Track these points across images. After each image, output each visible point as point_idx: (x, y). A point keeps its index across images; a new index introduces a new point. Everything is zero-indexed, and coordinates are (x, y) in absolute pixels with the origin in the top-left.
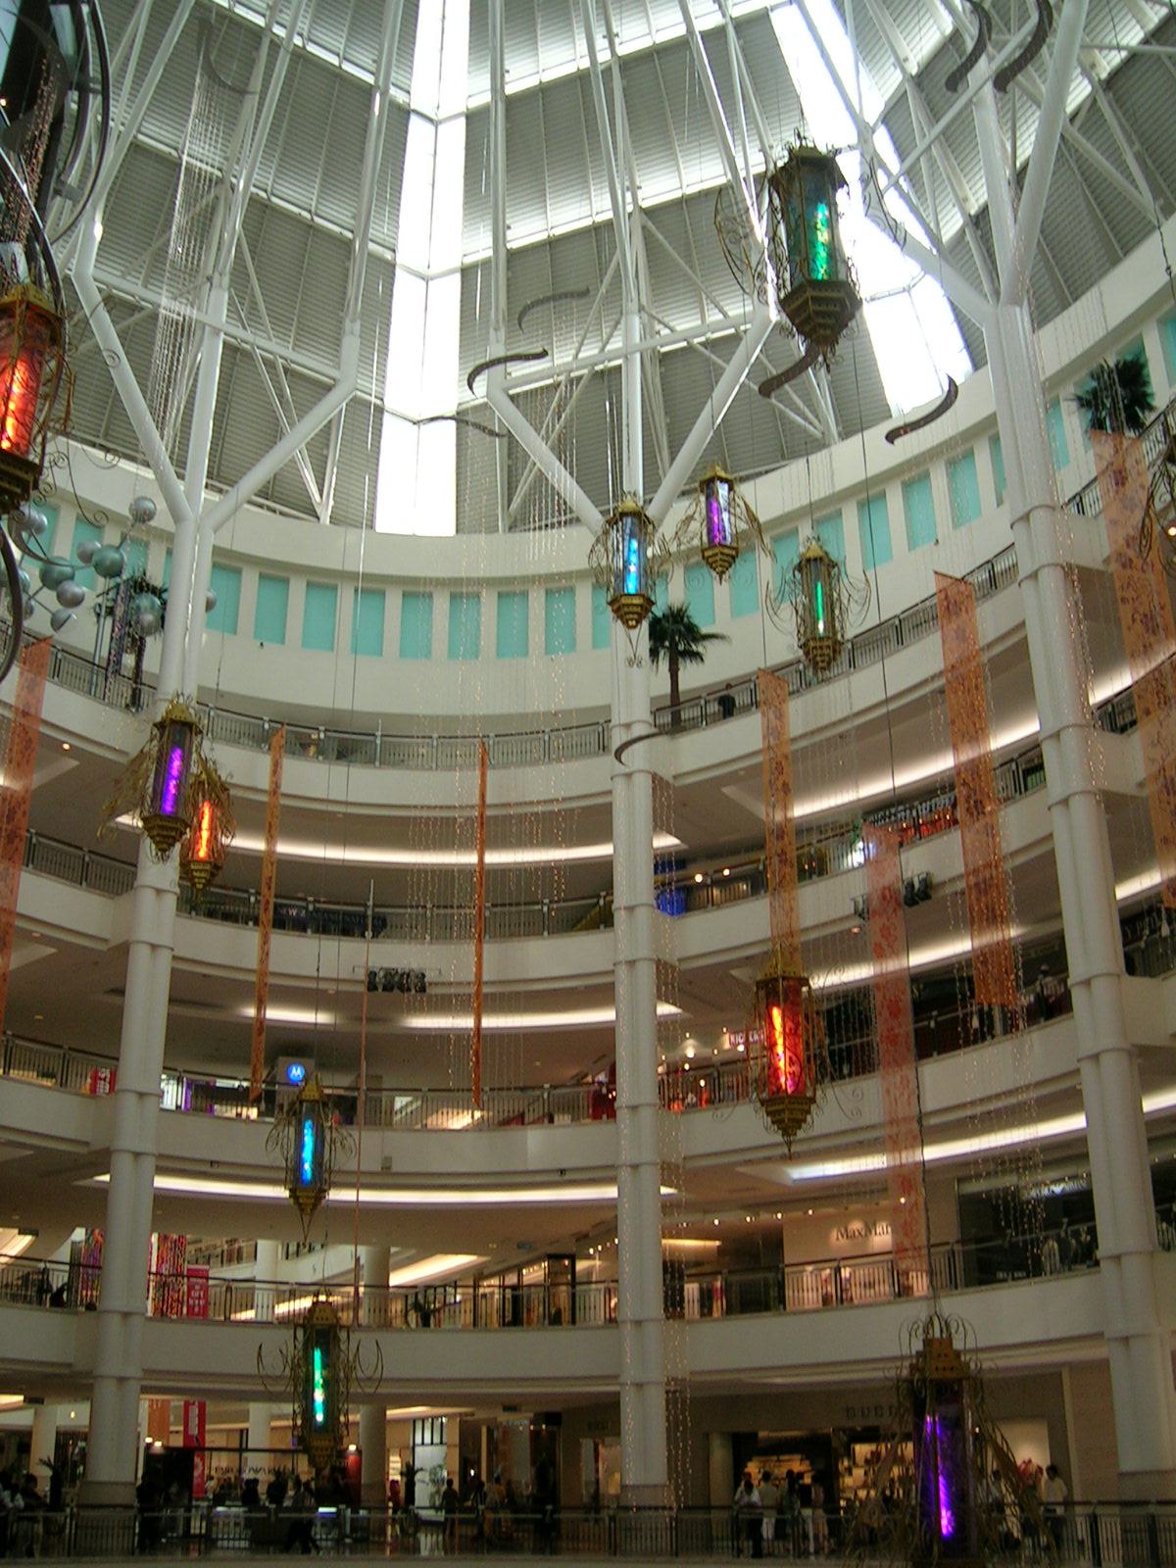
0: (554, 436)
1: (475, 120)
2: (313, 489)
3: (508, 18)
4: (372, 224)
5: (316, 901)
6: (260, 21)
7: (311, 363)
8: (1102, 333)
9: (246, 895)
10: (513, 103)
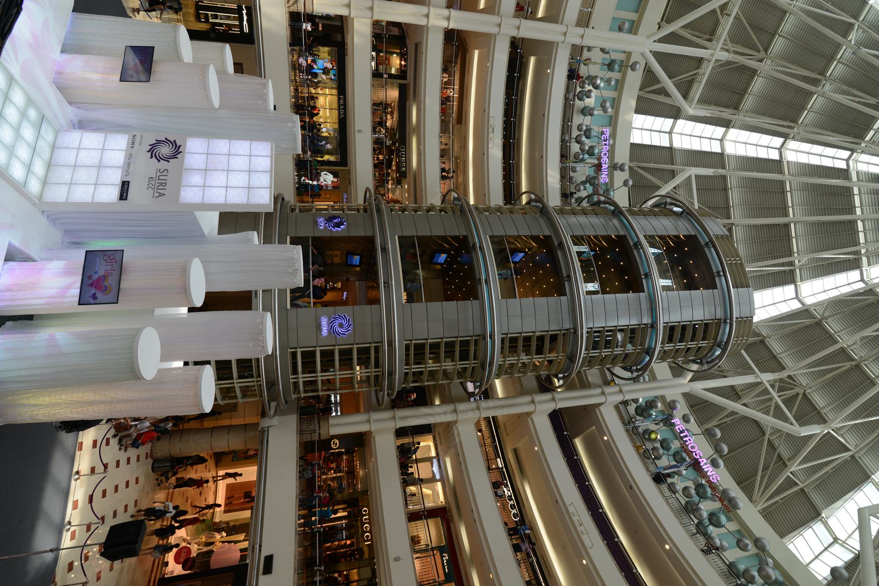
7: (698, 90)
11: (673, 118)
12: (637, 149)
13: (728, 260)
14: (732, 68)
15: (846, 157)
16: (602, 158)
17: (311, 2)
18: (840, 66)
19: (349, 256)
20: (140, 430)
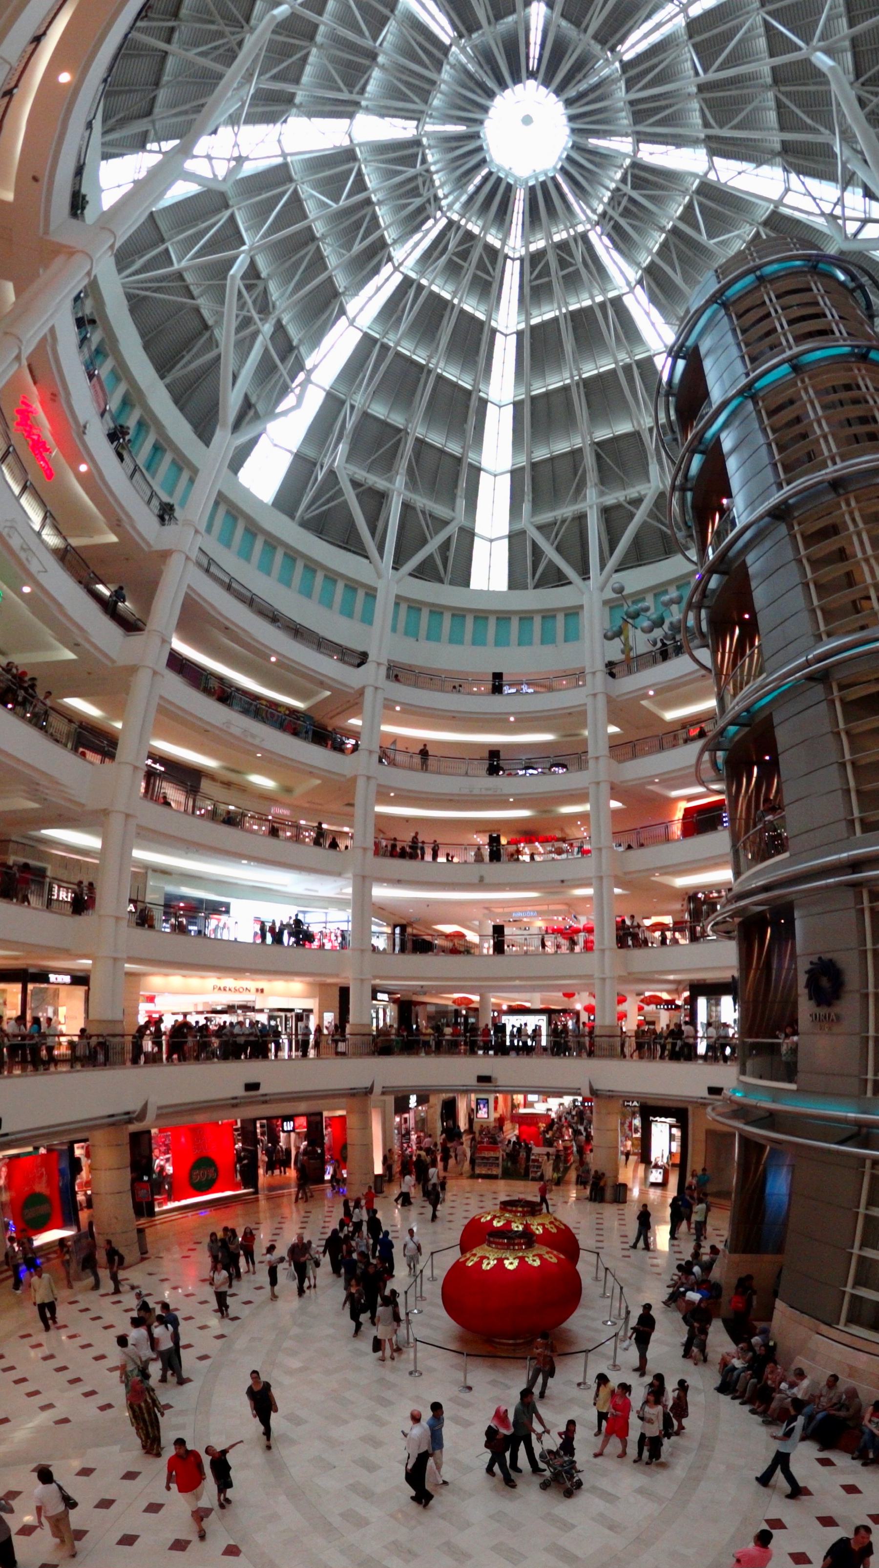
0: (556, 543)
1: (520, 334)
2: (441, 567)
3: (533, 367)
6: (424, 362)
7: (440, 510)
10: (534, 399)
12: (515, 582)
17: (876, 1352)
18: (403, 343)
20: (412, 1261)
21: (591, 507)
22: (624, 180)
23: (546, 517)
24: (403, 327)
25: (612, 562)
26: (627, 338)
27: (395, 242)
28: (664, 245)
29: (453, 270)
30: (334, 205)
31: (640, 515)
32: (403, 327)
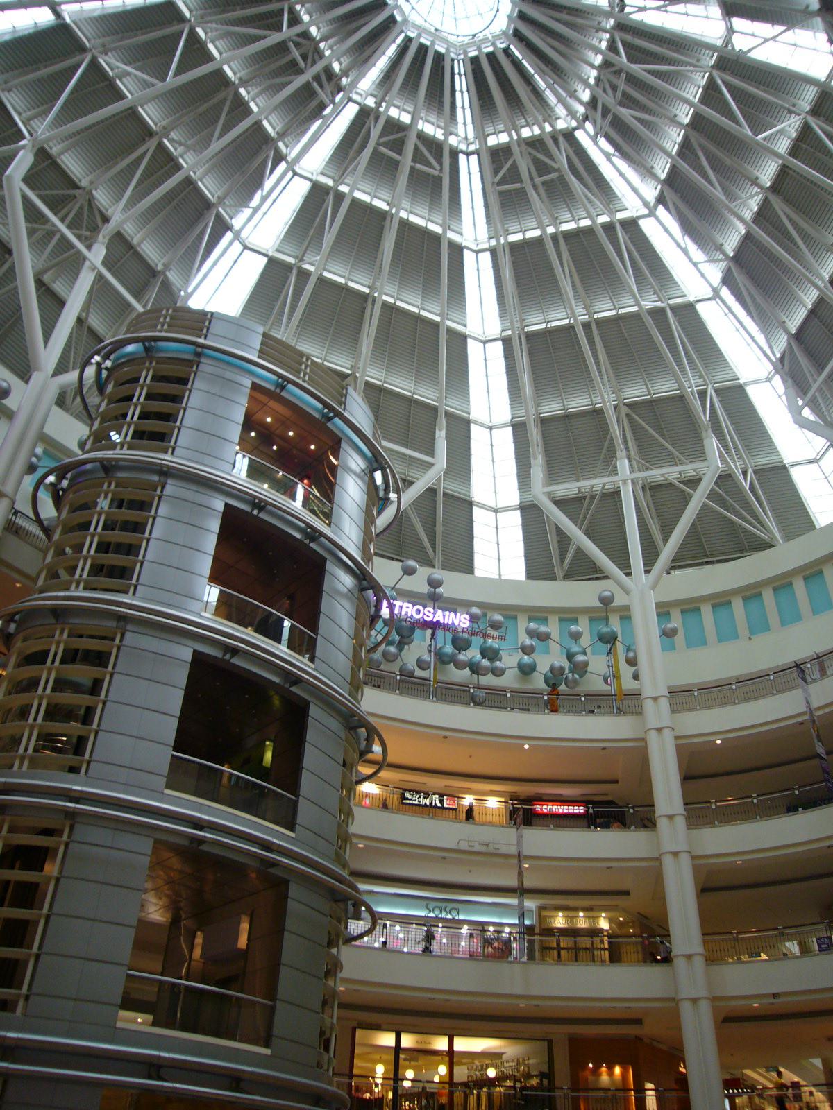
4: (92, 305)
5: (717, 801)
6: (367, 290)
8: (322, 609)
9: (709, 805)
11: (472, 509)
13: (163, 326)
14: (683, 491)
15: (465, 157)
16: (414, 605)
19: (34, 576)
21: (625, 482)
22: (612, 47)
23: (568, 489)
24: (329, 237)
25: (667, 551)
26: (701, 358)
27: (282, 135)
28: (685, 146)
29: (383, 168)
30: (160, 84)
31: (698, 499)
32: (329, 237)
